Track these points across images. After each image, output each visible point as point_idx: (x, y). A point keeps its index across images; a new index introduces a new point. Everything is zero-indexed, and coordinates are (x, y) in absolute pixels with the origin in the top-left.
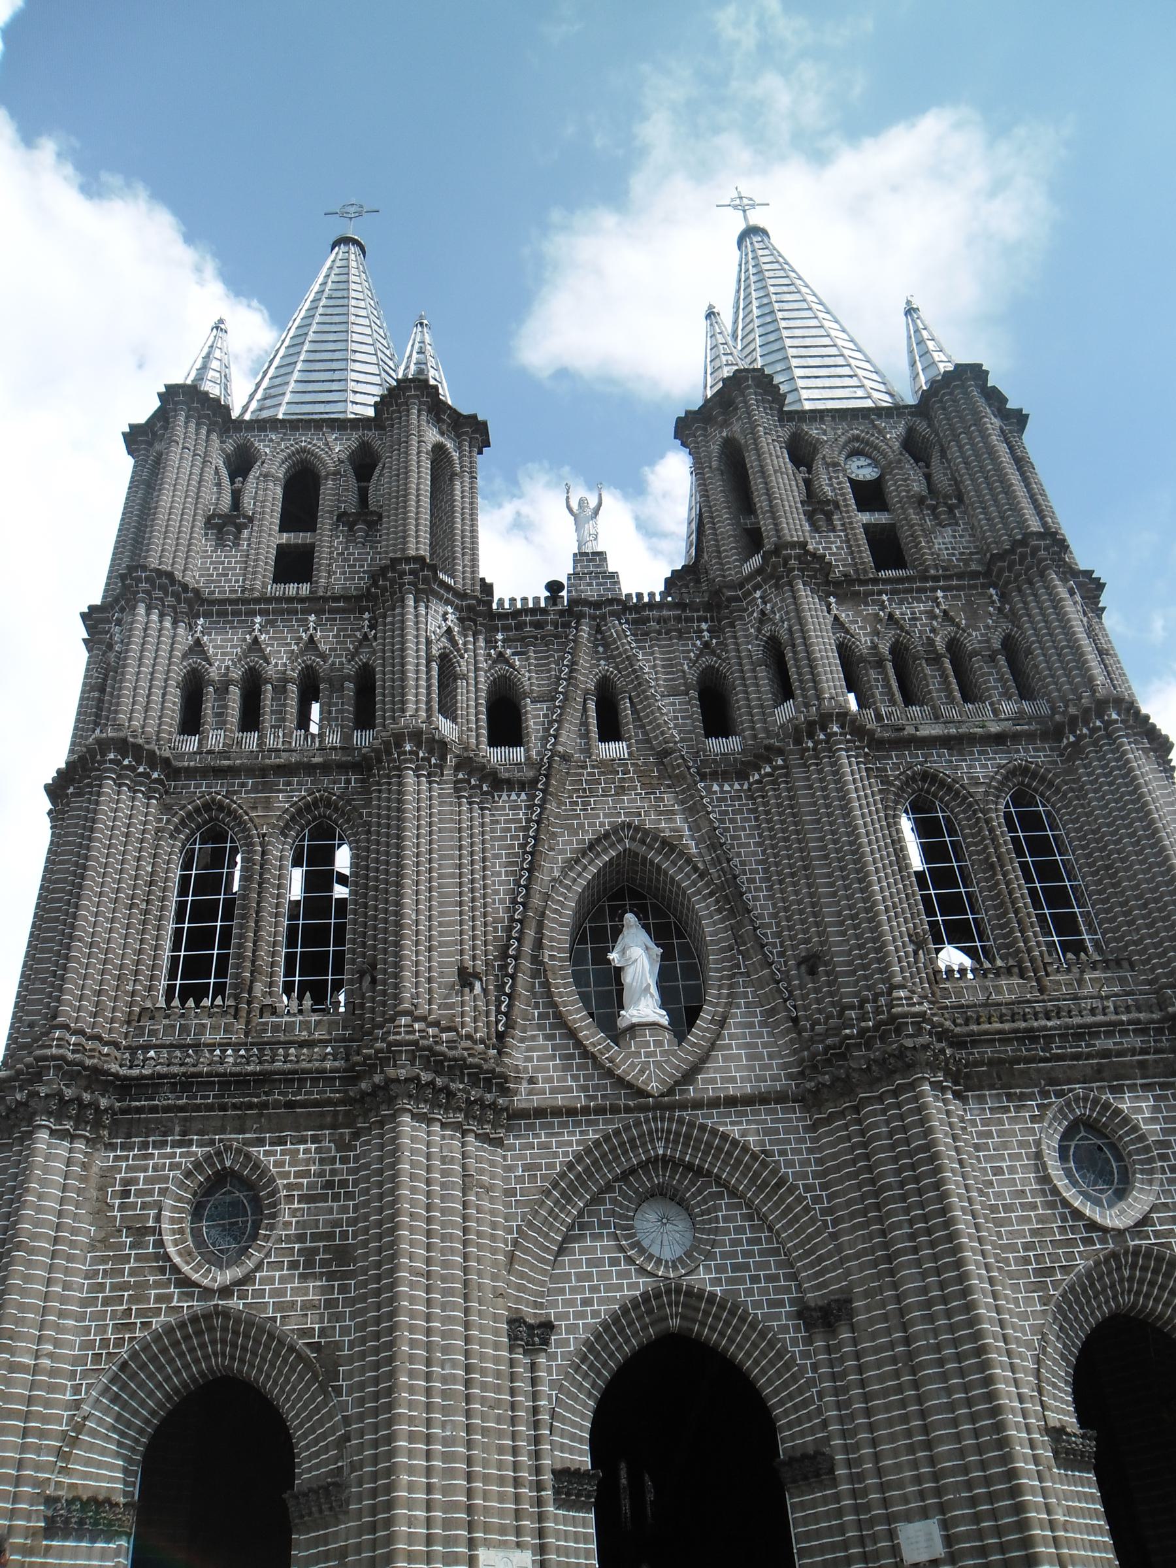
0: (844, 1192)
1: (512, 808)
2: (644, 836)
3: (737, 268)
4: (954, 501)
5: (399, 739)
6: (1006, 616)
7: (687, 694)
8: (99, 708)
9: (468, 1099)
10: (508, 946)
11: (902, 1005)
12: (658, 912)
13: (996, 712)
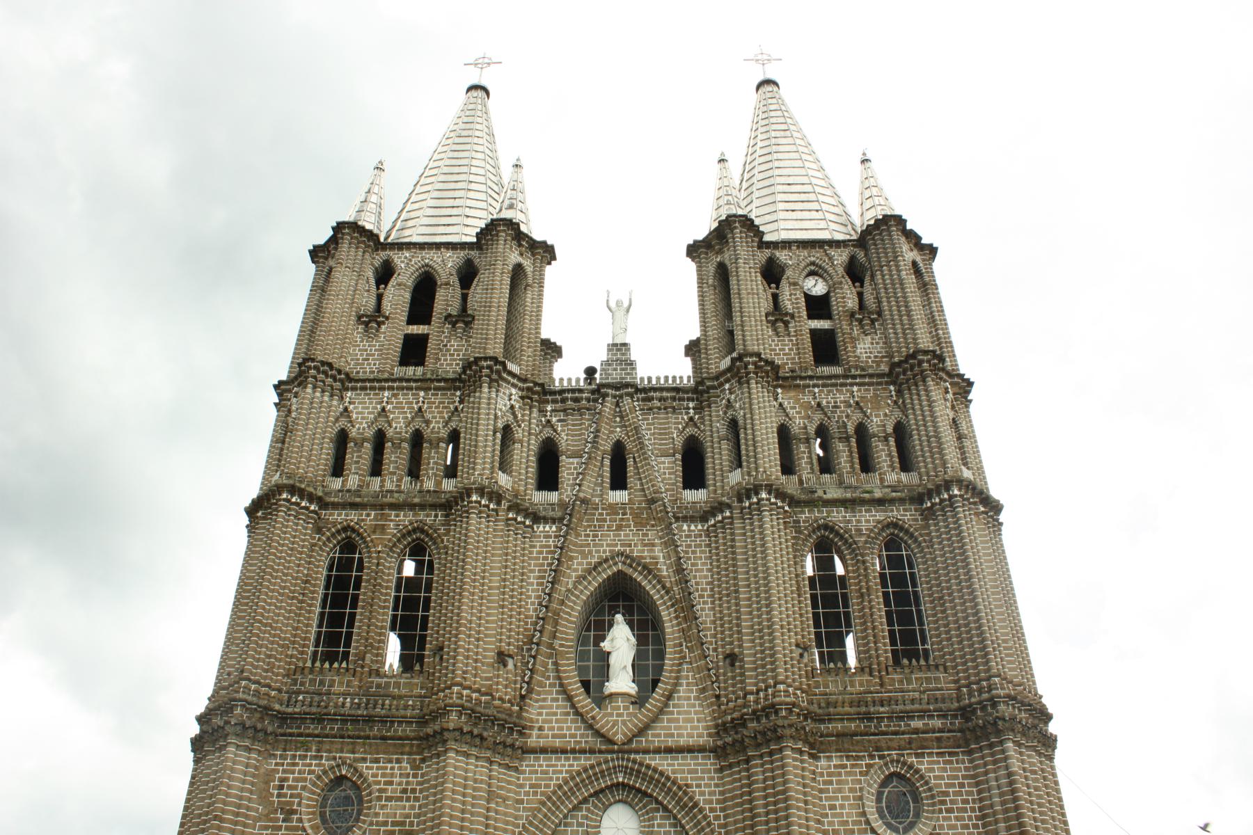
0: (734, 815)
1: (545, 537)
2: (630, 559)
3: (752, 115)
4: (875, 316)
5: (468, 491)
6: (899, 407)
7: (674, 456)
8: (281, 455)
9: (495, 742)
10: (534, 636)
11: (781, 696)
12: (642, 611)
13: (882, 480)
